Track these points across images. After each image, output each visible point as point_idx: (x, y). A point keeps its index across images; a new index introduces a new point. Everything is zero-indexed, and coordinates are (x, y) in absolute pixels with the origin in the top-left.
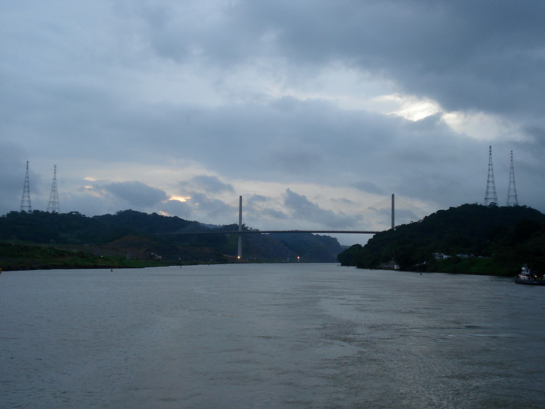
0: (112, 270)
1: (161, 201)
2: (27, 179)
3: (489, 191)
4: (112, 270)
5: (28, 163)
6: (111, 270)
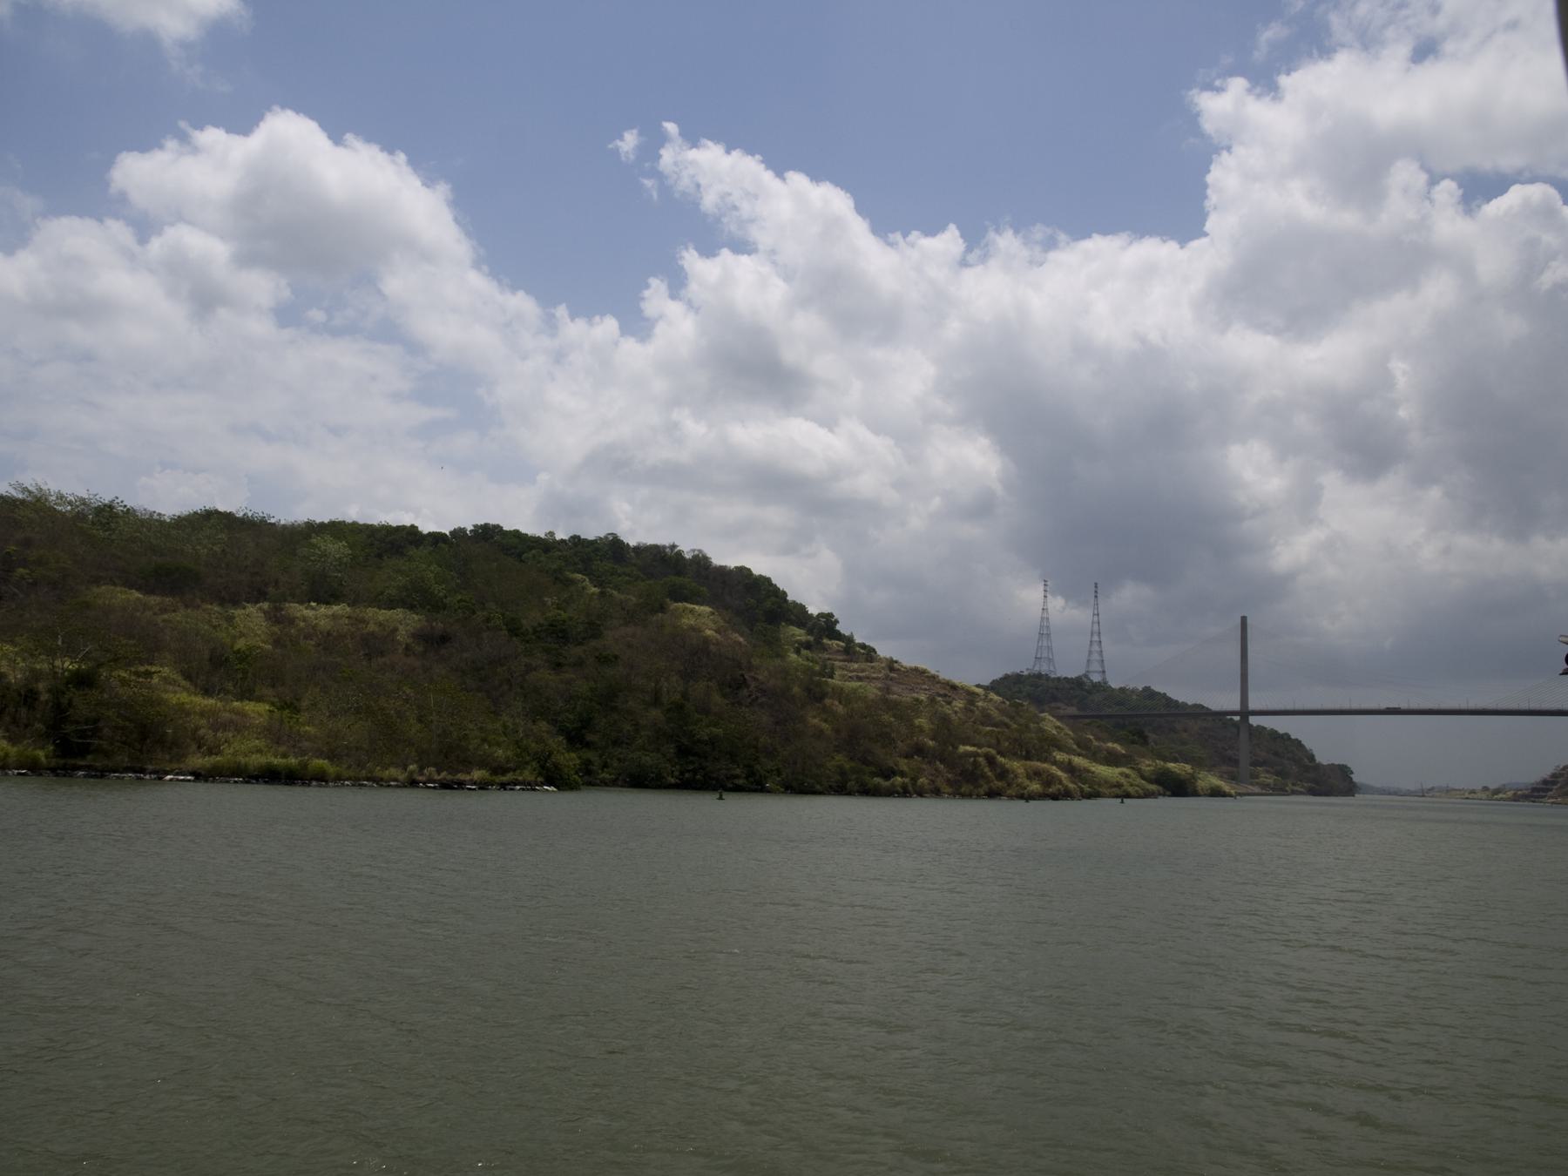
1: (825, 626)
3: (1093, 650)
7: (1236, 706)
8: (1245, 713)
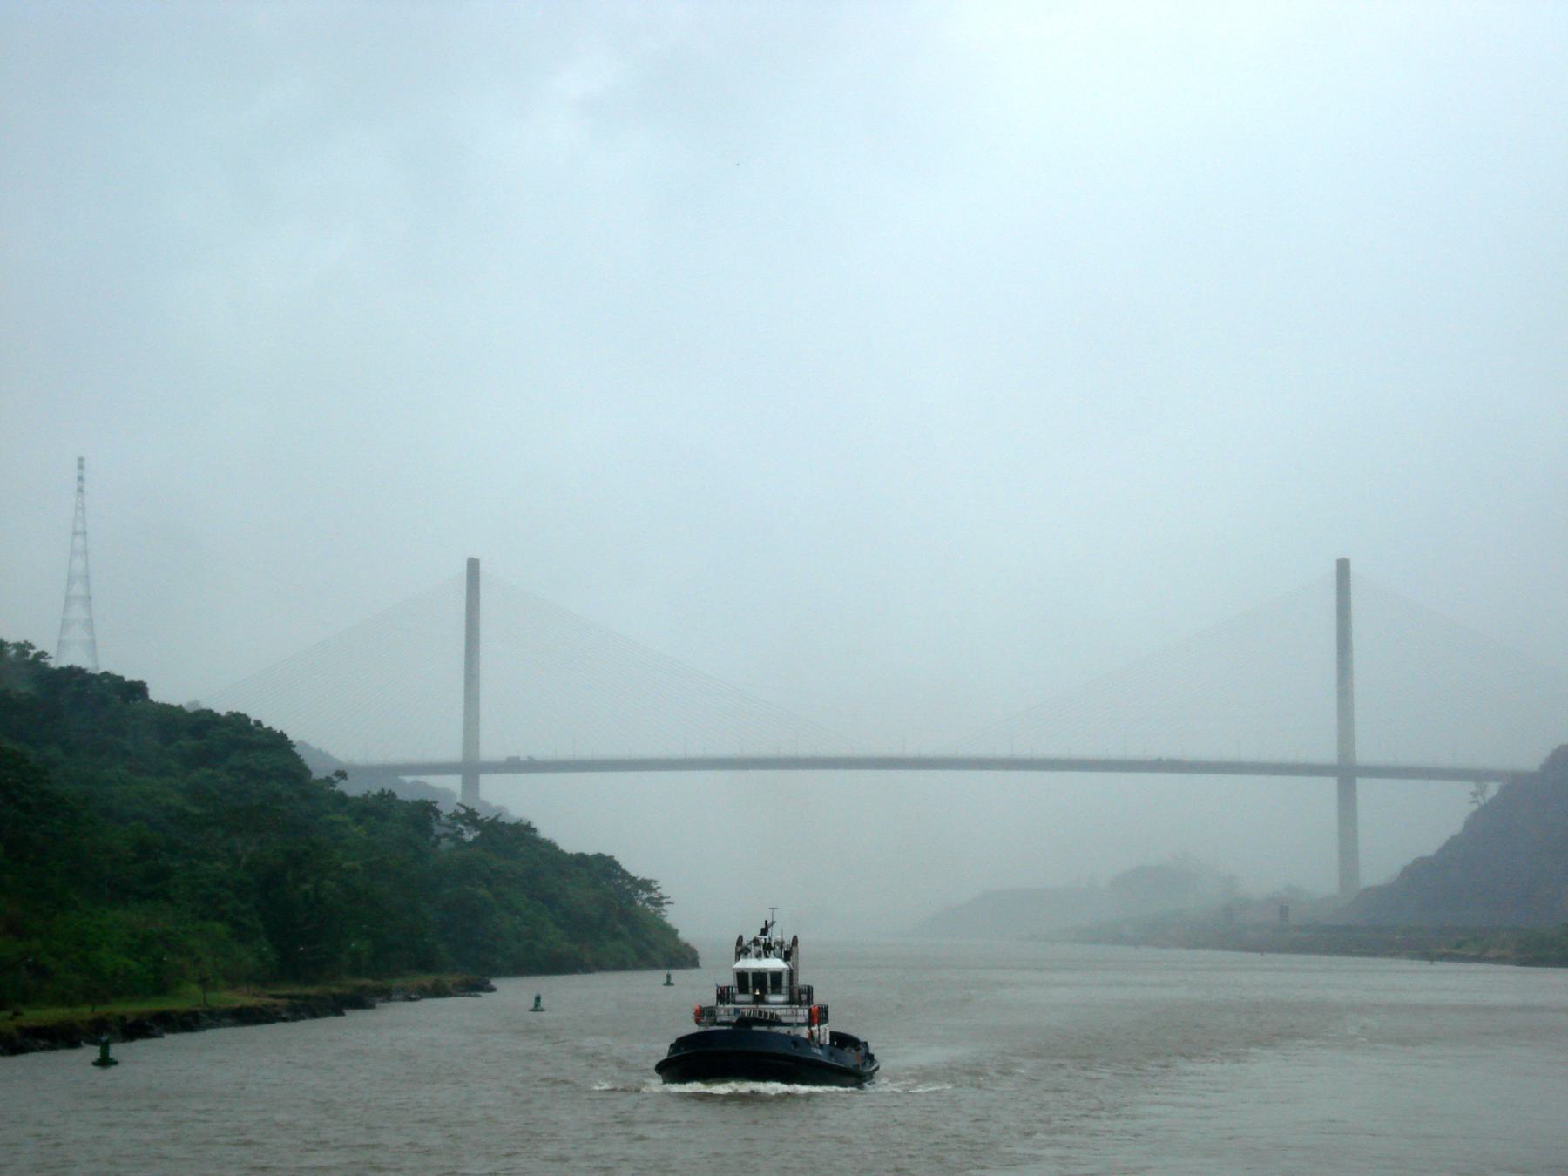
0: (669, 977)
2: (79, 541)
4: (669, 977)
5: (81, 467)
6: (665, 981)
7: (453, 752)
8: (471, 769)
